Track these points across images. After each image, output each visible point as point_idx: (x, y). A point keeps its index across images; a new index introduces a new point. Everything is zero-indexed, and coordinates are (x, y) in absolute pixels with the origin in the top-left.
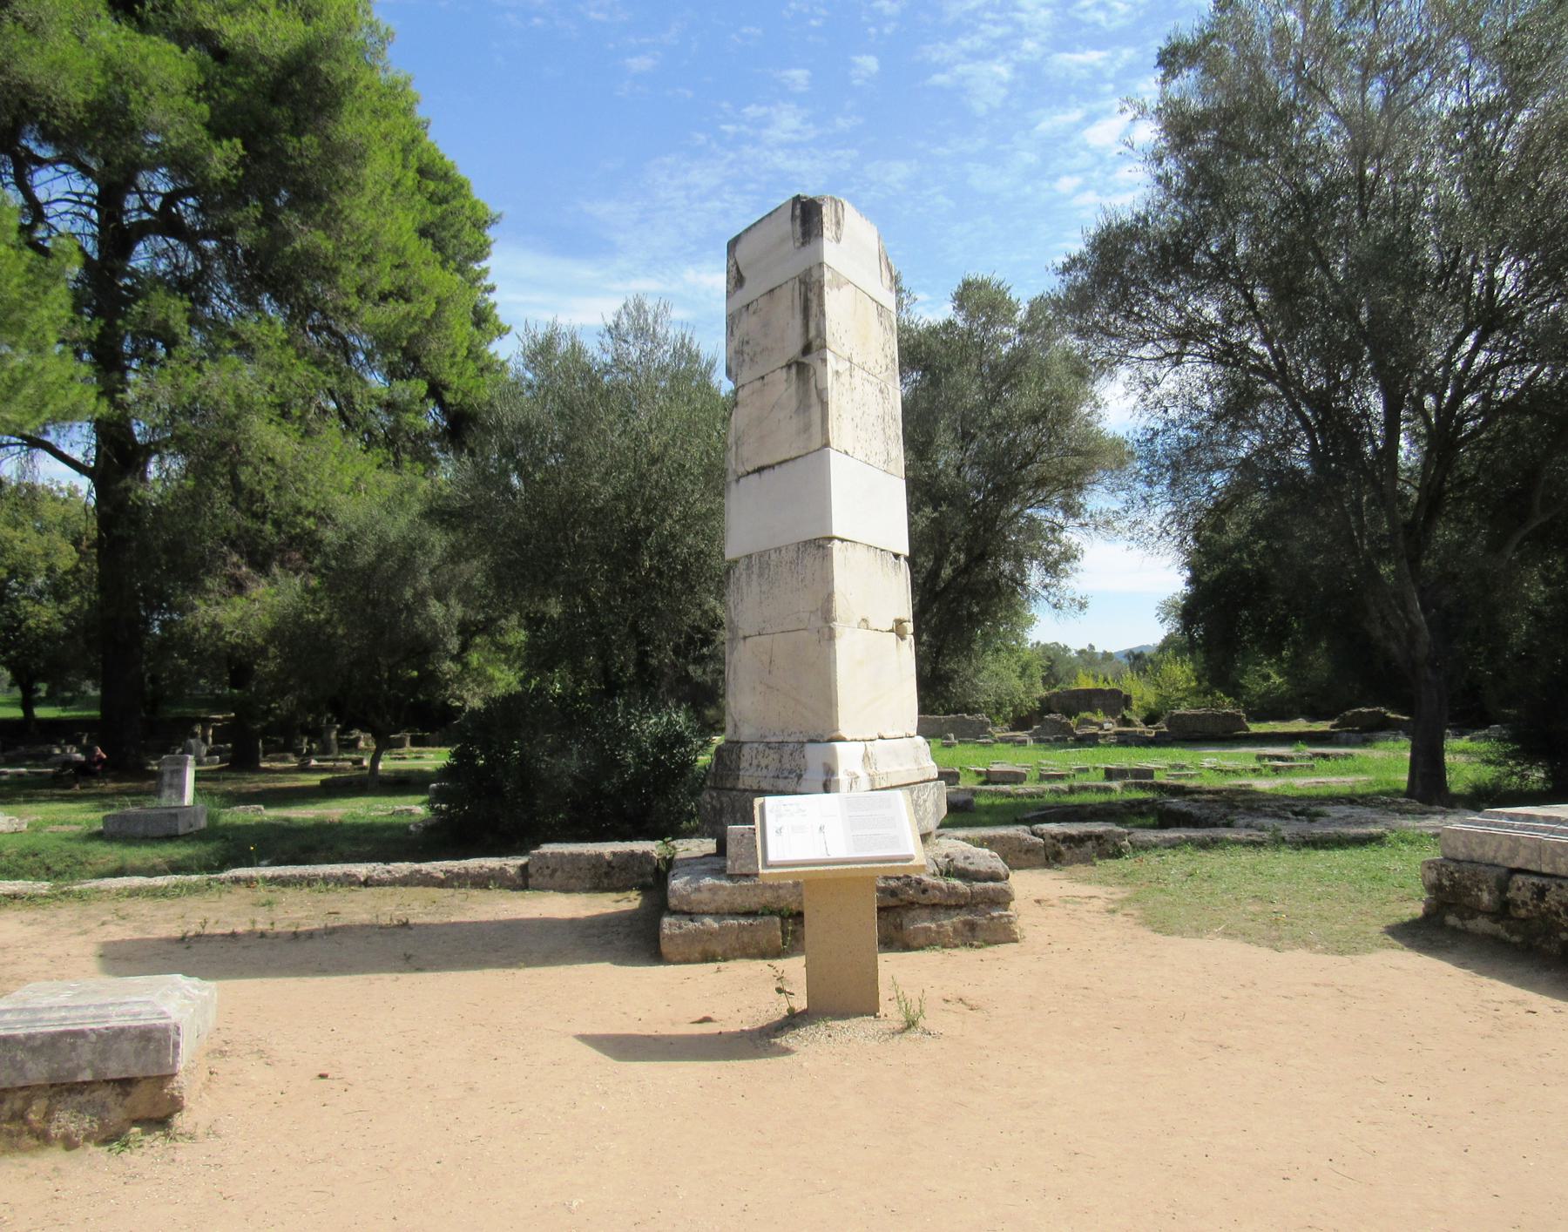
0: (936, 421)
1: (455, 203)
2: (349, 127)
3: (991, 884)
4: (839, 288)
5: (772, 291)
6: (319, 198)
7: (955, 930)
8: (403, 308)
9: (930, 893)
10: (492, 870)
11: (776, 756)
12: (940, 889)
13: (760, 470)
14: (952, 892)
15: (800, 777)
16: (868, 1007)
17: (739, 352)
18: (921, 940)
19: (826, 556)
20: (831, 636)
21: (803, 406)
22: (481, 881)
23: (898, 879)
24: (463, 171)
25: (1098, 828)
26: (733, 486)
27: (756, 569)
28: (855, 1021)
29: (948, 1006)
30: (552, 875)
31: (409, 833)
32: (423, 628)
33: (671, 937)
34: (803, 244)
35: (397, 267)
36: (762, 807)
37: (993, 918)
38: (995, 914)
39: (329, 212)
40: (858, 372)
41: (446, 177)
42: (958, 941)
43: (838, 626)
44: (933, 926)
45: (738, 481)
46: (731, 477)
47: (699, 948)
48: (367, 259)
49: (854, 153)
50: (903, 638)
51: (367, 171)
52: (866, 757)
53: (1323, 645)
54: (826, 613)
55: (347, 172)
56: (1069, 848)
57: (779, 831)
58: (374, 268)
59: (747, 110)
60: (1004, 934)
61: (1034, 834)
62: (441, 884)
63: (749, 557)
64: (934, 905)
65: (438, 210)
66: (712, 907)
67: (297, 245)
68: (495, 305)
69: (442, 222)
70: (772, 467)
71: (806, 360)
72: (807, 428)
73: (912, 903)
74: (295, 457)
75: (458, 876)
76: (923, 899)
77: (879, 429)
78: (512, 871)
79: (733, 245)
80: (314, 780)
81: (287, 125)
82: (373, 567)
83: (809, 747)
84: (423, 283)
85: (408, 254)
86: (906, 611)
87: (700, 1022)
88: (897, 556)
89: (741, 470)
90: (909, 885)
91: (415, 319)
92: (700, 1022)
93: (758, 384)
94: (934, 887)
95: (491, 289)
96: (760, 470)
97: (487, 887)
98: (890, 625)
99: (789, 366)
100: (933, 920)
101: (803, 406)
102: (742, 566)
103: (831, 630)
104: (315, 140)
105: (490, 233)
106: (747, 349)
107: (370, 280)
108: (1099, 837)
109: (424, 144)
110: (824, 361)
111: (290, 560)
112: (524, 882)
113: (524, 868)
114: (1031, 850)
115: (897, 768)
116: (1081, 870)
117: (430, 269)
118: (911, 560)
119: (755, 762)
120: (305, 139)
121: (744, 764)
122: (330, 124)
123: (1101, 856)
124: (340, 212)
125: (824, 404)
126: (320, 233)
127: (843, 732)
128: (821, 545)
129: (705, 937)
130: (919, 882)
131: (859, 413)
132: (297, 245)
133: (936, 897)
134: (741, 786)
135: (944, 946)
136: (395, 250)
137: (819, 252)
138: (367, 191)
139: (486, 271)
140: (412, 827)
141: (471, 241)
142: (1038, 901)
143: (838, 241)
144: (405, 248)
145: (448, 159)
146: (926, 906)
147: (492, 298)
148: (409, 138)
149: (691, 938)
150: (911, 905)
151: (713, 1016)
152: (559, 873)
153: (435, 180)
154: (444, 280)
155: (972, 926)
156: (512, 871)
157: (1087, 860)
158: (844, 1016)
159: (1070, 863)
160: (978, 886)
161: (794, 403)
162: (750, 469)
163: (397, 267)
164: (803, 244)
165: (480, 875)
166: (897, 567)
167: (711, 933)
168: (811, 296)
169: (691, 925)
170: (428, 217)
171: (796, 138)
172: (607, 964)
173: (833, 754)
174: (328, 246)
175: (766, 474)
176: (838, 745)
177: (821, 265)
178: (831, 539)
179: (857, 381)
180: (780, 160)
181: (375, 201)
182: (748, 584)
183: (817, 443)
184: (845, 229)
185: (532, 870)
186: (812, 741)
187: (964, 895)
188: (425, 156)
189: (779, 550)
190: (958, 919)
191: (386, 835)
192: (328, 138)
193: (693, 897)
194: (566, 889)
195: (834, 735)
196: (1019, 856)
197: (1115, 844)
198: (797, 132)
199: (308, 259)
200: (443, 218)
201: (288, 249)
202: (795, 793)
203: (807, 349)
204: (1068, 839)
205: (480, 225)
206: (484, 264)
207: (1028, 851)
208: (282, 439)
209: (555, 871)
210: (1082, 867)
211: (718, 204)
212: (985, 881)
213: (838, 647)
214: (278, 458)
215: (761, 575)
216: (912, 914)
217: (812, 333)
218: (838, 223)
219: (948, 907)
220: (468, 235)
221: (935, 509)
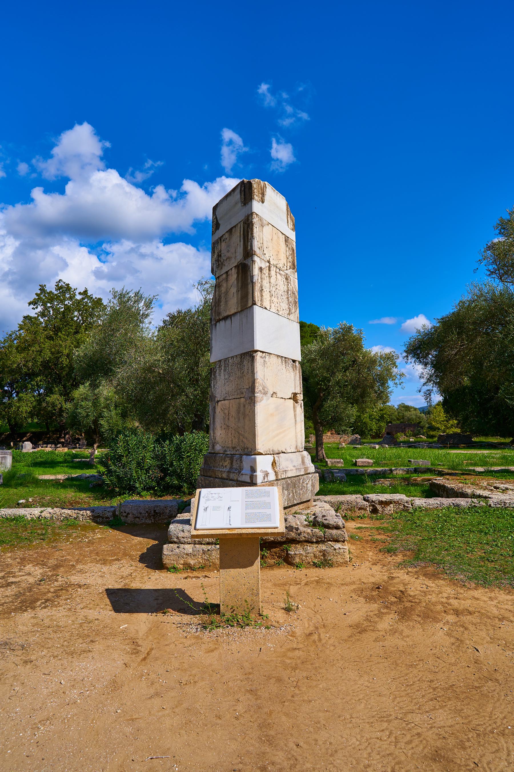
5: (231, 229)
17: (218, 260)
19: (252, 359)
36: (200, 492)
40: (273, 269)
50: (297, 402)
52: (274, 464)
53: (251, 167)
57: (206, 509)
61: (364, 499)
63: (220, 361)
77: (285, 297)
79: (215, 208)
86: (298, 388)
88: (294, 361)
98: (290, 395)
110: (253, 261)
128: (249, 355)
131: (274, 289)
143: (263, 202)
152: (130, 515)
166: (294, 368)
173: (255, 460)
177: (252, 214)
179: (273, 273)
182: (220, 375)
184: (266, 198)
209: (128, 514)
215: (225, 370)
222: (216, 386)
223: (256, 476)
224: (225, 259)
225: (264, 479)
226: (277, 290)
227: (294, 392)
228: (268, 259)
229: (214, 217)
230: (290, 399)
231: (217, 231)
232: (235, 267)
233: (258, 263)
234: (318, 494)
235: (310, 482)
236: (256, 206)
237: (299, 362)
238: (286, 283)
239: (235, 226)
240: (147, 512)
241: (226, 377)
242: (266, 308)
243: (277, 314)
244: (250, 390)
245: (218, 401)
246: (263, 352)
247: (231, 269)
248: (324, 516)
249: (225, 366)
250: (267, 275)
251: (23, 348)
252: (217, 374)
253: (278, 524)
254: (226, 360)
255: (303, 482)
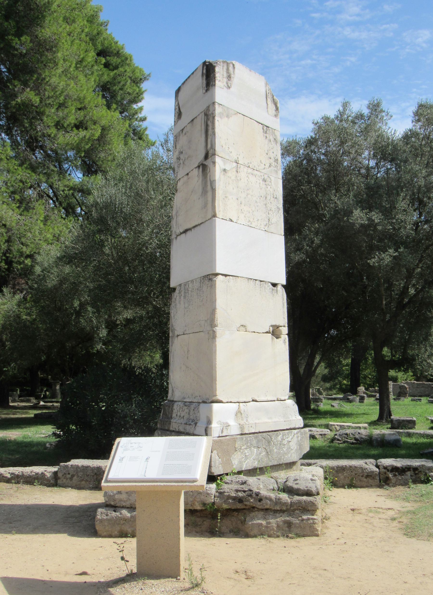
0: (398, 195)
1: (121, 69)
2: (48, 30)
3: (305, 498)
4: (228, 116)
5: (193, 120)
6: (32, 72)
7: (278, 526)
8: (82, 133)
9: (264, 502)
10: (37, 474)
11: (187, 411)
12: (270, 499)
13: (185, 231)
14: (278, 501)
15: (196, 424)
16: (173, 573)
18: (255, 531)
19: (213, 287)
20: (213, 336)
21: (204, 192)
22: (30, 480)
23: (244, 491)
24: (127, 51)
25: (416, 463)
26: (174, 240)
27: (183, 293)
28: (162, 580)
29: (236, 576)
30: (71, 479)
31: (46, 448)
32: (85, 324)
33: (101, 521)
34: (207, 91)
35: (80, 109)
37: (303, 520)
38: (305, 517)
39: (38, 79)
40: (244, 171)
41: (118, 54)
42: (279, 534)
43: (219, 330)
44: (264, 523)
45: (176, 238)
46: (174, 236)
47: (118, 528)
48: (61, 106)
49: (395, 26)
51: (59, 55)
52: (239, 413)
54: (212, 322)
55: (49, 55)
56: (395, 475)
57: (121, 459)
58: (66, 111)
59: (328, 4)
60: (309, 531)
62: (8, 481)
63: (180, 285)
64: (267, 509)
65: (112, 74)
66: (128, 504)
67: (19, 100)
68: (146, 129)
69: (114, 81)
70: (190, 229)
71: (205, 163)
72: (205, 206)
73: (254, 508)
74: (17, 223)
75: (18, 476)
76: (259, 505)
78: (48, 475)
80: (31, 414)
81: (13, 31)
82: (56, 288)
83: (202, 405)
84: (95, 118)
85: (86, 101)
87: (81, 574)
88: (274, 285)
89: (178, 232)
90: (251, 496)
91: (89, 139)
92: (81, 574)
93: (186, 178)
94: (266, 498)
95: (144, 119)
96: (185, 231)
97: (33, 484)
99: (199, 167)
100: (265, 519)
101: (204, 192)
102: (177, 291)
103: (214, 332)
104: (29, 38)
105: (144, 86)
106: (182, 157)
107: (64, 118)
108: (415, 469)
109: (104, 35)
110: (214, 163)
111: (18, 284)
112: (55, 482)
113: (55, 473)
114: (370, 475)
115: (267, 420)
116: (400, 490)
117: (98, 109)
118: (288, 288)
119: (179, 414)
120: (23, 38)
121: (174, 415)
122: (39, 29)
123: (415, 482)
124: (44, 79)
125: (213, 190)
126: (33, 93)
127: (219, 397)
129: (122, 522)
130: (257, 494)
132: (19, 100)
133: (267, 504)
134: (171, 429)
135: (270, 536)
136: (80, 100)
137: (213, 96)
138: (60, 65)
139: (141, 109)
140: (48, 445)
141: (130, 91)
142: (353, 510)
144: (84, 98)
145: (120, 43)
146: (262, 510)
147: (144, 124)
148: (95, 32)
149: (114, 522)
150: (253, 509)
151: (89, 572)
152: (75, 478)
153: (109, 55)
154: (109, 116)
155: (289, 524)
156: (48, 475)
157: (405, 484)
158: (157, 577)
159: (394, 486)
160: (296, 498)
161: (200, 190)
162: (181, 231)
163: (80, 109)
164: (207, 91)
165: (30, 477)
167: (125, 520)
168: (210, 123)
169: (114, 514)
170: (106, 78)
171: (357, 19)
172: (66, 535)
174: (36, 100)
175: (189, 233)
176: (215, 406)
178: (217, 274)
180: (347, 32)
181: (65, 72)
182: (180, 303)
183: (209, 216)
184: (235, 80)
185: (60, 475)
186: (204, 402)
187: (285, 504)
188: (106, 42)
189: (192, 281)
190: (281, 519)
191: (34, 449)
192: (37, 37)
193: (117, 497)
194: (79, 488)
195: (214, 398)
196: (336, 479)
197: (426, 474)
198: (358, 15)
199: (26, 106)
200: (114, 79)
201: (14, 103)
202: (194, 435)
203: (206, 157)
204: (394, 469)
205: (137, 81)
206: (140, 105)
207: (367, 476)
208: (10, 213)
209: (73, 476)
210: (401, 488)
211: (309, 61)
212: (303, 495)
213: (217, 343)
214: (8, 224)
215: (185, 297)
216: (253, 514)
217: (209, 146)
218: (229, 77)
219: (276, 511)
220: (129, 87)
221: (396, 250)
222: (176, 317)
223: (211, 428)
224: (186, 157)
225: (222, 432)
226: (249, 196)
227: (274, 324)
228: (235, 158)
229: (177, 104)
230: (267, 332)
231: (179, 121)
232: (196, 168)
233: (219, 164)
234: (306, 456)
235: (295, 439)
236: (220, 93)
237: (283, 286)
238: (264, 186)
239: (196, 117)
240: (96, 474)
241: (186, 305)
242: (231, 220)
243: (249, 226)
244: (209, 321)
245: (178, 336)
246: (226, 275)
247: (192, 170)
248: (296, 480)
249: (185, 292)
250: (233, 178)
251: (374, 195)
252: (177, 302)
253: (198, 476)
254: (186, 284)
255: (283, 439)
